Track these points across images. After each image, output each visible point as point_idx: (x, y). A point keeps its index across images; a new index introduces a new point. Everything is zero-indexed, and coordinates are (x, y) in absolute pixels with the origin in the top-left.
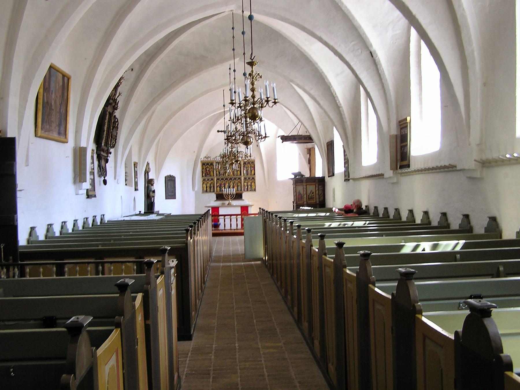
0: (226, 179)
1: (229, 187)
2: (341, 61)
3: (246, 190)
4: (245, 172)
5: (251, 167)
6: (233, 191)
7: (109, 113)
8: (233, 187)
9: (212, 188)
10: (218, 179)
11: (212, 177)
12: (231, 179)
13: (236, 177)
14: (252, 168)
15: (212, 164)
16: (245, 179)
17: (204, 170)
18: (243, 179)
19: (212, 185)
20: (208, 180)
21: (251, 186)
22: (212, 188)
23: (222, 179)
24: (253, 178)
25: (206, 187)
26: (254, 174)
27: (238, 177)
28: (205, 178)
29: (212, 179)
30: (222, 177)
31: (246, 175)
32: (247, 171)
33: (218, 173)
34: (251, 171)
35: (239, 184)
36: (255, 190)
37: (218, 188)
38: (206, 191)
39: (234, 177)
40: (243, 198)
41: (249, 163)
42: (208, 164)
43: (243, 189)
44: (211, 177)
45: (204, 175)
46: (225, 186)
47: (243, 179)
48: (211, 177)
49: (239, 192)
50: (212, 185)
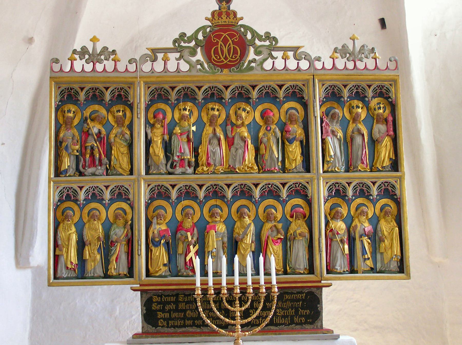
0: (216, 193)
1: (233, 246)
2: (74, 287)
3: (341, 264)
4: (334, 147)
5: (372, 119)
6: (270, 273)
7: (60, 141)
8: (260, 248)
9: (120, 250)
10: (159, 193)
11: (123, 180)
12: (244, 192)
13: (276, 178)
14: (380, 129)
15: (122, 98)
16: (337, 192)
17: (70, 135)
18: (321, 192)
19: (119, 232)
20: (95, 196)
21: (375, 238)
22: (120, 250)
23: (188, 193)
24: (391, 193)
25: (81, 244)
26: (395, 165)
27: (292, 178)
28: (74, 181)
29: (121, 195)
30: (185, 178)
31: (340, 166)
32: (347, 143)
33: (158, 150)
34: (374, 143)
35: (298, 227)
36: (402, 267)
37: (161, 254)
38: (81, 273)
39: (265, 179)
40: (327, 321)
41: (359, 95)
42: (95, 96)
43: (321, 261)
44: (114, 181)
45: (67, 163)
46: (202, 243)
47: (321, 192)
48: (114, 181)
49: (301, 278)
50: (119, 232)
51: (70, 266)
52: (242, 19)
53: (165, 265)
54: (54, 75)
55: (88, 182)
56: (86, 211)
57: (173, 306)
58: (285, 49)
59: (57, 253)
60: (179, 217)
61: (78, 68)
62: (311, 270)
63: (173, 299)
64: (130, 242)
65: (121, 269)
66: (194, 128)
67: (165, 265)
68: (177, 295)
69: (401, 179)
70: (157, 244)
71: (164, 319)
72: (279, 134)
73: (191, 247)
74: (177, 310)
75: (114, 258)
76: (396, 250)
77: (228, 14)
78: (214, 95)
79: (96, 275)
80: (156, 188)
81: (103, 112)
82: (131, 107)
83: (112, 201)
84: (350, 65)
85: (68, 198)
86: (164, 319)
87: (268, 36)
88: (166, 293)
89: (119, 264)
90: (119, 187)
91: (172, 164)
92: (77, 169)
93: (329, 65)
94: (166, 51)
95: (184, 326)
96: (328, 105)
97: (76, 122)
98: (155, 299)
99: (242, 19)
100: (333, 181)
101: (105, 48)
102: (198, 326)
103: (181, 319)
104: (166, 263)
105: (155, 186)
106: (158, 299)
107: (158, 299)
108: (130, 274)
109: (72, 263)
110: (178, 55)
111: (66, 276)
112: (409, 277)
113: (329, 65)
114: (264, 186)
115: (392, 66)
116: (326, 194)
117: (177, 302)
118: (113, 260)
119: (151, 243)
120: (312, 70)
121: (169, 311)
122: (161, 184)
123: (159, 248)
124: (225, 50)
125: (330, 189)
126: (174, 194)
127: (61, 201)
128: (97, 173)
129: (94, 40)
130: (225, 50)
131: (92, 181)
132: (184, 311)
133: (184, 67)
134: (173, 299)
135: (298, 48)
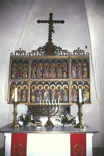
11: (26, 80)
24: (87, 83)
27: (64, 80)
52: (54, 44)
54: (11, 56)
55: (79, 80)
56: (78, 87)
57: (36, 109)
58: (63, 51)
60: (38, 88)
61: (17, 55)
62: (68, 102)
63: (36, 107)
66: (42, 68)
68: (37, 107)
69: (90, 81)
70: (33, 95)
71: (34, 112)
72: (61, 70)
73: (41, 96)
74: (36, 110)
76: (14, 97)
77: (51, 43)
78: (47, 61)
81: (22, 65)
82: (28, 63)
83: (23, 85)
84: (19, 55)
85: (13, 84)
86: (34, 112)
87: (59, 48)
88: (34, 106)
89: (24, 100)
91: (37, 76)
92: (16, 77)
93: (14, 55)
94: (36, 51)
95: (38, 114)
96: (73, 63)
97: (16, 67)
98: (32, 107)
99: (54, 44)
100: (74, 81)
101: (23, 50)
102: (41, 114)
103: (37, 112)
106: (32, 107)
107: (32, 107)
108: (27, 102)
110: (38, 52)
112: (91, 103)
113: (14, 55)
115: (87, 54)
116: (72, 84)
117: (36, 108)
120: (69, 55)
121: (35, 110)
124: (50, 50)
125: (73, 83)
126: (37, 83)
127: (12, 84)
129: (20, 49)
130: (50, 50)
131: (33, 80)
132: (38, 110)
133: (40, 55)
134: (36, 107)
135: (66, 50)
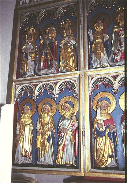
9: (67, 138)
51: (24, 154)
53: (110, 156)
59: (15, 142)
64: (76, 134)
65: (67, 162)
67: (110, 156)
70: (101, 134)
75: (61, 148)
79: (45, 164)
80: (99, 80)
90: (102, 79)
104: (111, 154)
105: (98, 79)
109: (26, 152)
111: (21, 163)
114: (61, 84)
118: (60, 150)
119: (95, 134)
122: (103, 76)
123: (104, 137)
128: (48, 73)
